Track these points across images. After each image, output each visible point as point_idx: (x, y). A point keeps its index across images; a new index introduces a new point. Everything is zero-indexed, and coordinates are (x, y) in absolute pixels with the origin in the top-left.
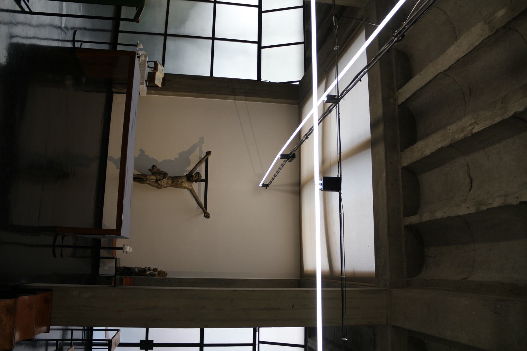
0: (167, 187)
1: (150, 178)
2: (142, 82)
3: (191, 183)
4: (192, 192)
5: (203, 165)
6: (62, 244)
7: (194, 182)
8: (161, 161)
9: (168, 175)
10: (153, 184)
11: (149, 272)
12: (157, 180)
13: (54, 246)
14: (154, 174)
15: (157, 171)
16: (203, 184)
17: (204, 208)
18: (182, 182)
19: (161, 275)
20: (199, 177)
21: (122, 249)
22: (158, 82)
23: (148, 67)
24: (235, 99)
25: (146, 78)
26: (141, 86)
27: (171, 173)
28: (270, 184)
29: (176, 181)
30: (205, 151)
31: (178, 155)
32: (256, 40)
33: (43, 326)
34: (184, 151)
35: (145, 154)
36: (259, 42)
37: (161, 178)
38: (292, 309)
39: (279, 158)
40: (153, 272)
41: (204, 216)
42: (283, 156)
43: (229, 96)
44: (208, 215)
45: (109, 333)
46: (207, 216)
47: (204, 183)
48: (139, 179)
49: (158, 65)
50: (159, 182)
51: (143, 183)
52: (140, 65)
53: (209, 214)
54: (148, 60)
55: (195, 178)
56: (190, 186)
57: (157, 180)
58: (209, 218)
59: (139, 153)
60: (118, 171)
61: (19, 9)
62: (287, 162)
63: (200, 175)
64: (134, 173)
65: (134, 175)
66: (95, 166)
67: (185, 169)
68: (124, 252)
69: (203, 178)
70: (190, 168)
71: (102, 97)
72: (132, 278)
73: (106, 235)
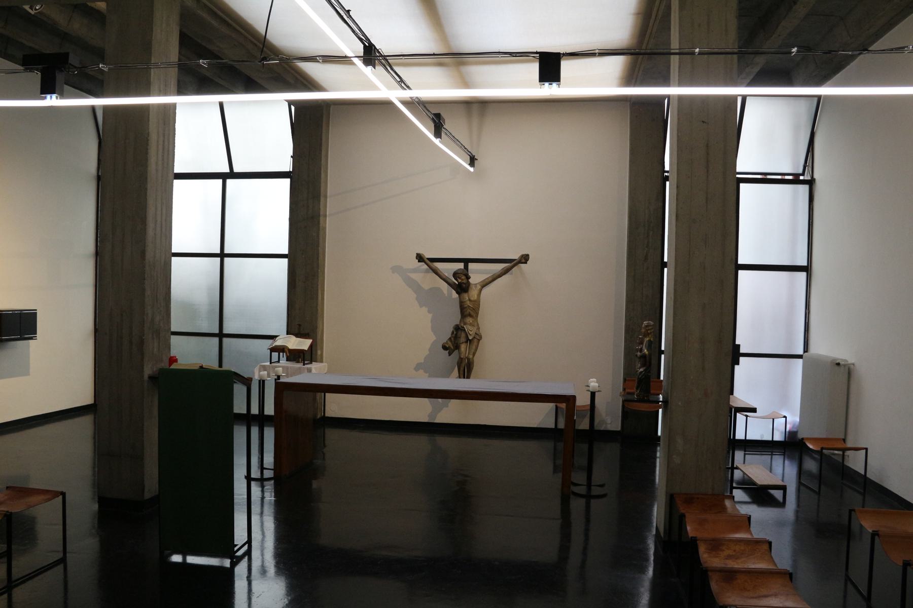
0: (478, 325)
1: (464, 353)
2: (306, 371)
3: (471, 286)
4: (485, 284)
5: (439, 266)
6: (585, 485)
7: (469, 282)
8: (434, 336)
9: (458, 323)
10: (474, 347)
11: (646, 350)
12: (468, 341)
13: (588, 497)
14: (457, 347)
15: (451, 341)
16: (471, 266)
17: (512, 263)
18: (470, 300)
19: (649, 332)
20: (461, 274)
21: (593, 395)
22: (304, 344)
23: (279, 361)
24: (325, 216)
25: (300, 365)
26: (314, 371)
27: (455, 318)
28: (472, 154)
29: (468, 311)
30: (416, 263)
31: (424, 308)
32: (219, 182)
33: (725, 506)
34: (417, 299)
35: (423, 361)
36: (224, 177)
37: (463, 335)
38: (708, 124)
39: (440, 142)
40: (644, 345)
41: (526, 263)
42: (438, 134)
43: (321, 225)
44: (524, 258)
46: (525, 259)
47: (469, 263)
48: (466, 369)
49: (276, 346)
50: (470, 338)
51: (473, 363)
52: (287, 376)
53: (522, 256)
54: (269, 363)
55: (462, 280)
56: (476, 287)
57: (468, 341)
58: (528, 255)
59: (421, 371)
60: (454, 403)
62: (444, 127)
63: (457, 270)
64: (457, 378)
65: (460, 377)
66: (446, 442)
67: (446, 295)
68: (599, 391)
69: (461, 266)
70: (444, 286)
71: (332, 436)
72: (627, 379)
73: (575, 418)
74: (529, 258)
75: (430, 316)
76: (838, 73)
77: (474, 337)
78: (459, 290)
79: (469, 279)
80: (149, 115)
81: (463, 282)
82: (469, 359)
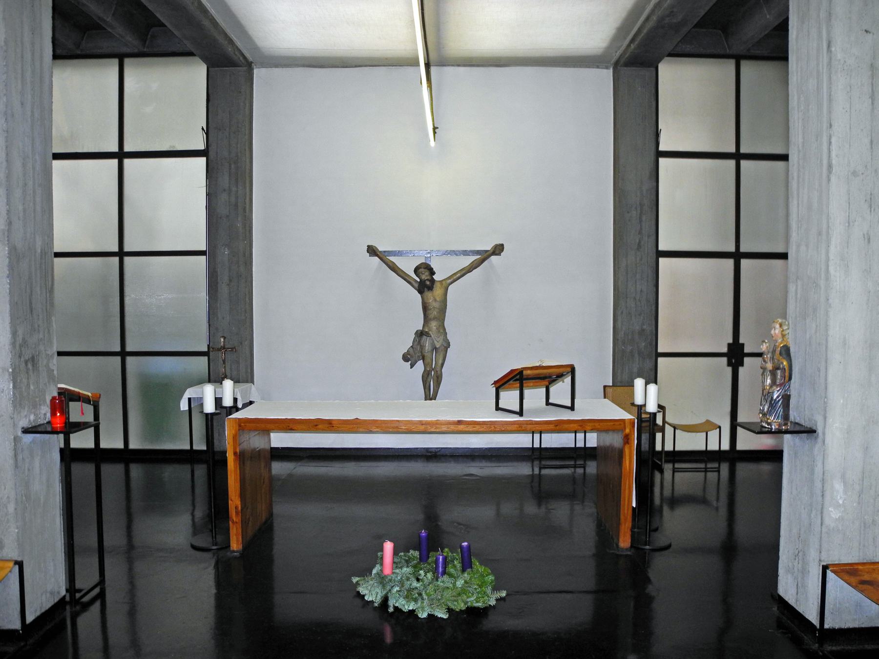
45: (543, 389)
46: (498, 250)
61: (98, 604)
79: (434, 275)
80: (222, 29)
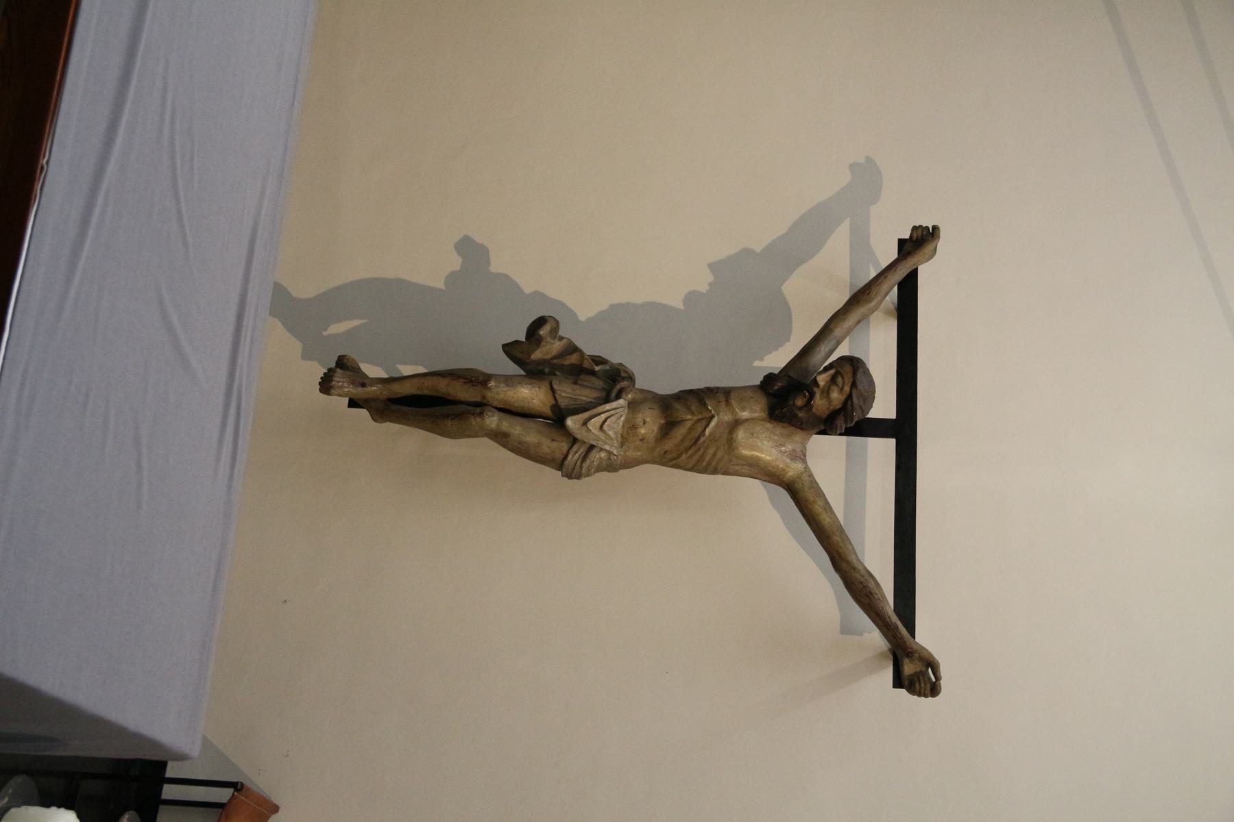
0: (627, 464)
3: (799, 436)
14: (535, 372)
15: (562, 355)
16: (883, 450)
17: (895, 619)
18: (736, 423)
20: (854, 385)
34: (747, 253)
41: (898, 682)
47: (893, 441)
53: (931, 663)
55: (826, 392)
69: (884, 406)
74: (920, 694)
75: (676, 301)
76: (61, 758)
77: (575, 440)
78: (778, 385)
81: (818, 396)
82: (480, 406)
